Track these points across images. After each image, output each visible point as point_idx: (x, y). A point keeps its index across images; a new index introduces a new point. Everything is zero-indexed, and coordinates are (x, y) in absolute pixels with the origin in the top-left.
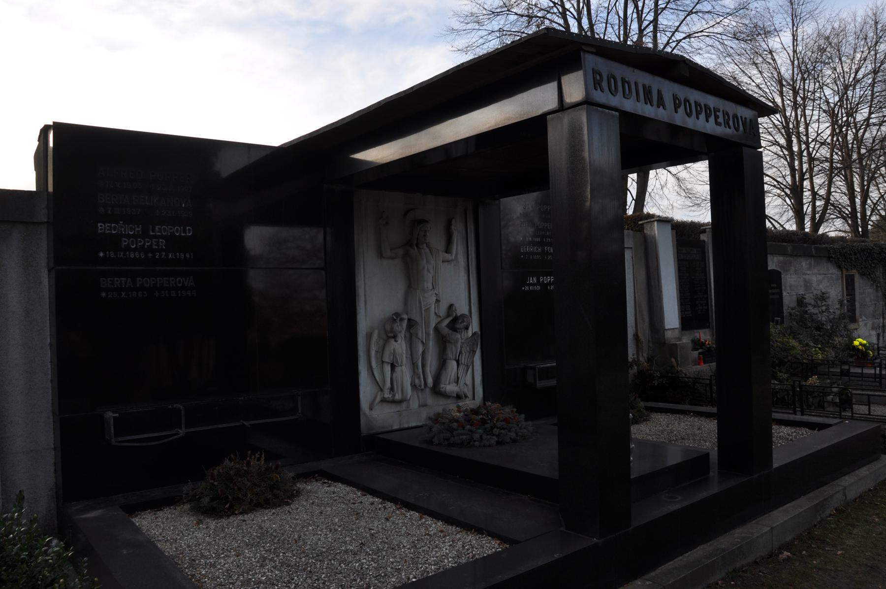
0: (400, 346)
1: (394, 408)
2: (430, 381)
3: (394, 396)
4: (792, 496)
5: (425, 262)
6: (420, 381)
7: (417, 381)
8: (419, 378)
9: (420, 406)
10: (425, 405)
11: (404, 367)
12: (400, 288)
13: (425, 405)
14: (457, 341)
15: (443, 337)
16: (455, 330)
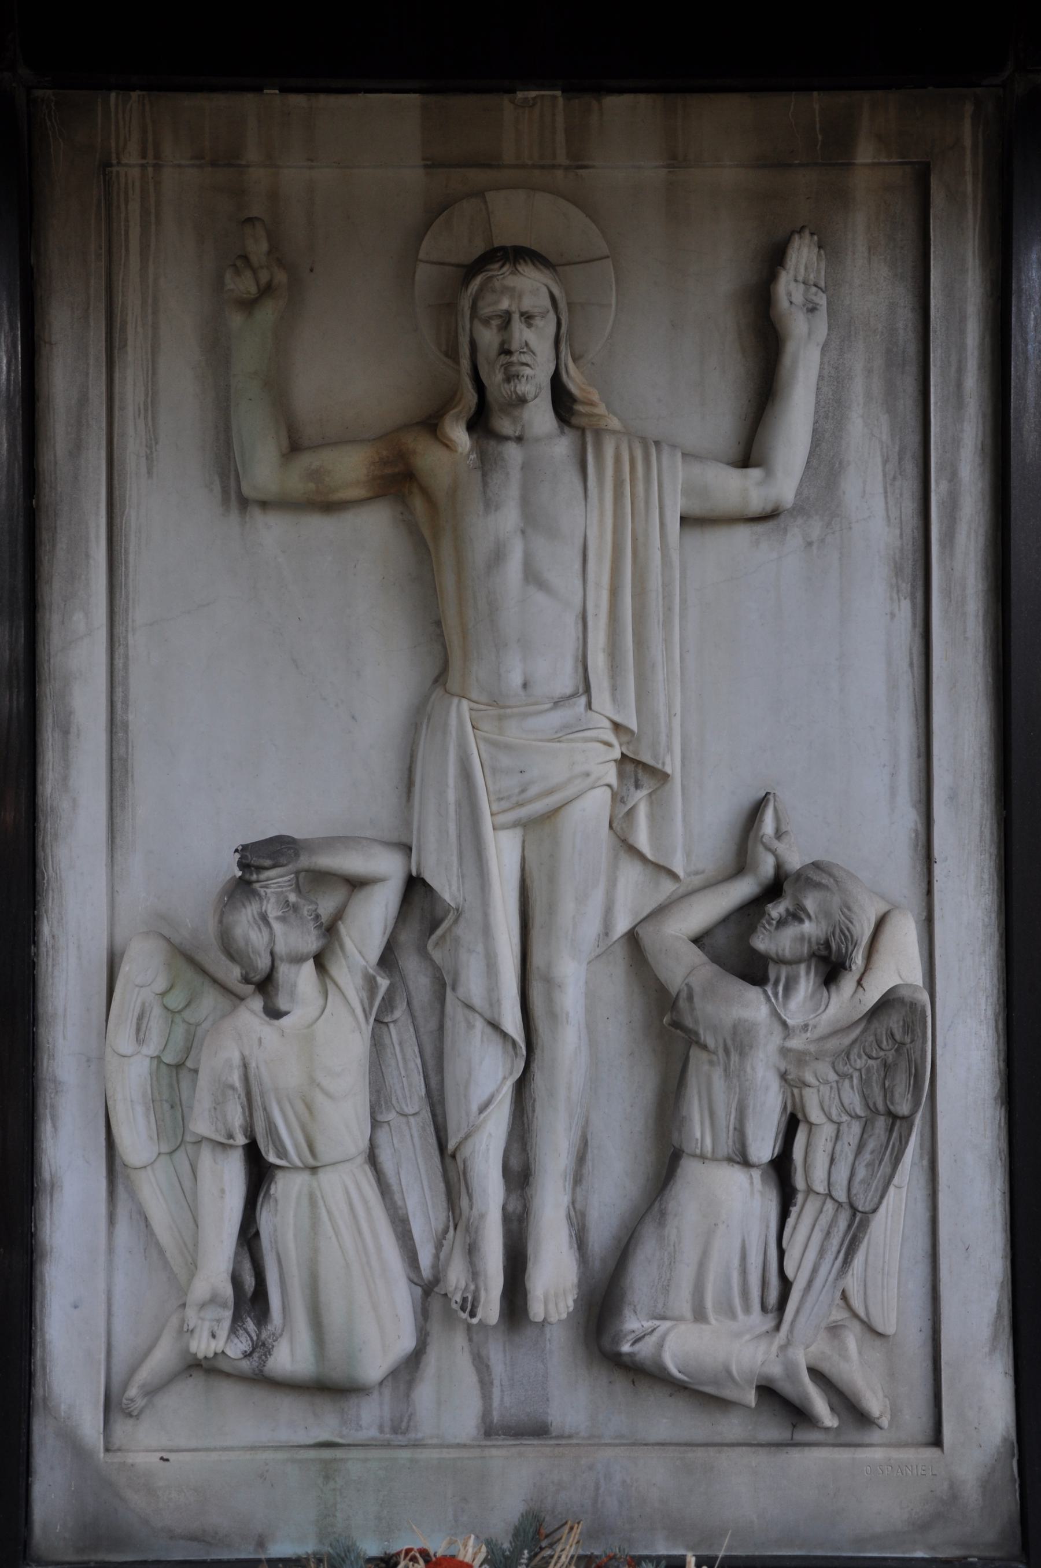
0: (318, 1050)
1: (300, 1424)
2: (555, 1278)
3: (261, 1348)
4: (929, 224)
5: (508, 518)
6: (475, 1274)
7: (456, 1277)
8: (472, 1251)
9: (489, 1430)
10: (537, 1430)
11: (330, 1182)
12: (383, 678)
13: (537, 1430)
14: (739, 1042)
15: (183, 1063)
16: (754, 970)
